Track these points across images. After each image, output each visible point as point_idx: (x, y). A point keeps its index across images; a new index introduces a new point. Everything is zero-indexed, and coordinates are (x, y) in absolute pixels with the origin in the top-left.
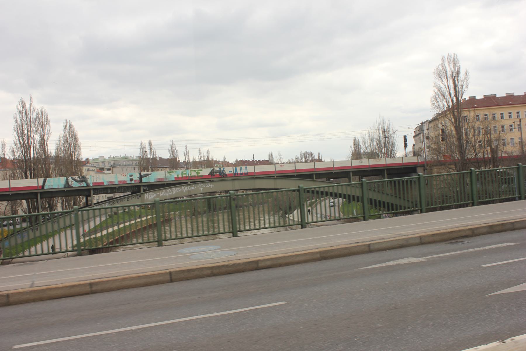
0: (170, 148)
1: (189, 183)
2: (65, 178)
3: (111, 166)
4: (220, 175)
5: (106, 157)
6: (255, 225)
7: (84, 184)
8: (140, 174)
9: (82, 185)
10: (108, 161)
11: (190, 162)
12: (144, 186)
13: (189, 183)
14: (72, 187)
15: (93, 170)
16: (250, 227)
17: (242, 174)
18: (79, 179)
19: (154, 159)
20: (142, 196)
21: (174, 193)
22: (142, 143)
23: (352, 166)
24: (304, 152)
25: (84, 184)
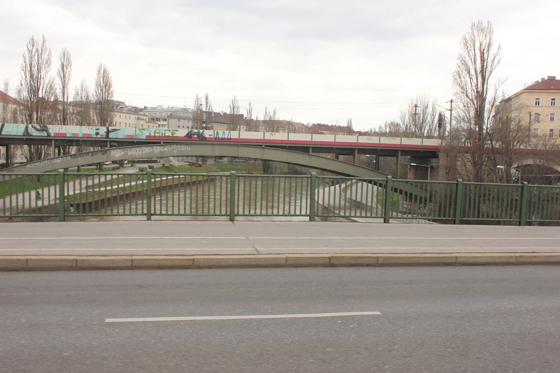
0: (231, 105)
1: (162, 144)
2: (25, 125)
3: (168, 117)
4: (198, 138)
5: (165, 107)
6: (161, 210)
7: (45, 134)
8: (108, 129)
9: (43, 135)
10: (166, 111)
11: (259, 121)
12: (111, 141)
13: (162, 144)
14: (32, 136)
15: (143, 120)
16: (255, 211)
17: (224, 139)
18: (39, 128)
19: (209, 114)
20: (108, 152)
21: (144, 152)
22: (197, 96)
23: (357, 143)
24: (389, 122)
25: (45, 134)
